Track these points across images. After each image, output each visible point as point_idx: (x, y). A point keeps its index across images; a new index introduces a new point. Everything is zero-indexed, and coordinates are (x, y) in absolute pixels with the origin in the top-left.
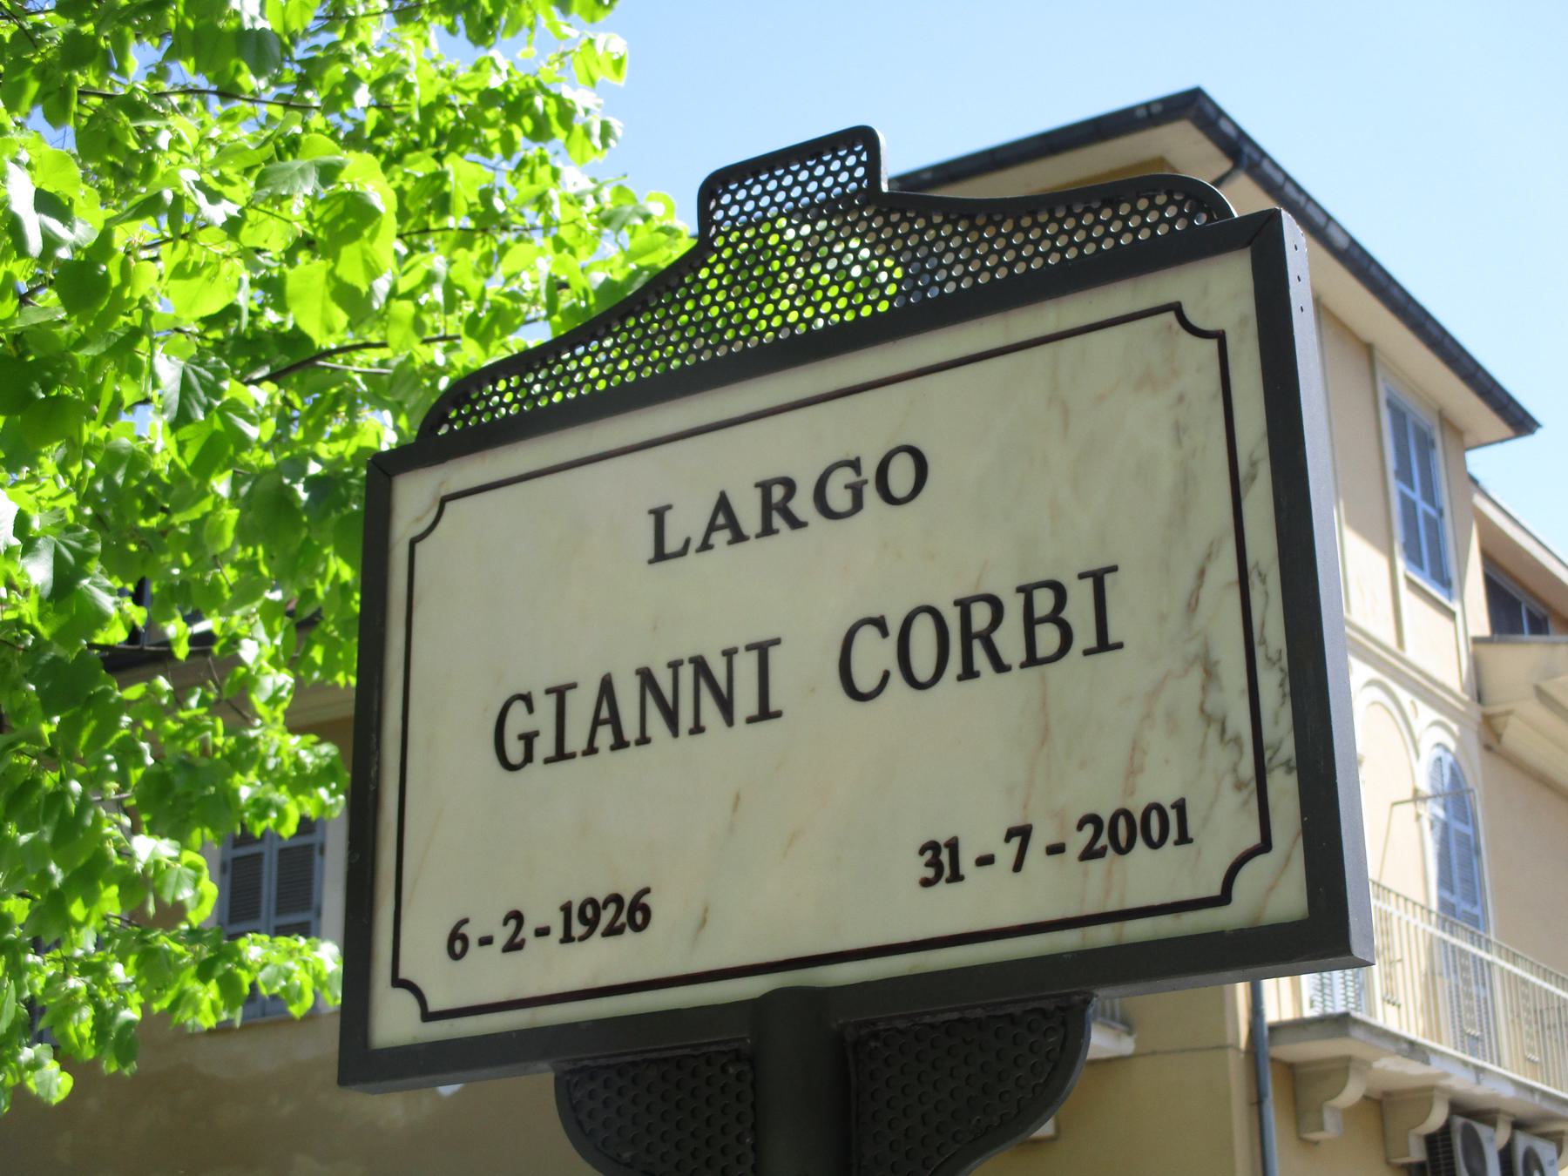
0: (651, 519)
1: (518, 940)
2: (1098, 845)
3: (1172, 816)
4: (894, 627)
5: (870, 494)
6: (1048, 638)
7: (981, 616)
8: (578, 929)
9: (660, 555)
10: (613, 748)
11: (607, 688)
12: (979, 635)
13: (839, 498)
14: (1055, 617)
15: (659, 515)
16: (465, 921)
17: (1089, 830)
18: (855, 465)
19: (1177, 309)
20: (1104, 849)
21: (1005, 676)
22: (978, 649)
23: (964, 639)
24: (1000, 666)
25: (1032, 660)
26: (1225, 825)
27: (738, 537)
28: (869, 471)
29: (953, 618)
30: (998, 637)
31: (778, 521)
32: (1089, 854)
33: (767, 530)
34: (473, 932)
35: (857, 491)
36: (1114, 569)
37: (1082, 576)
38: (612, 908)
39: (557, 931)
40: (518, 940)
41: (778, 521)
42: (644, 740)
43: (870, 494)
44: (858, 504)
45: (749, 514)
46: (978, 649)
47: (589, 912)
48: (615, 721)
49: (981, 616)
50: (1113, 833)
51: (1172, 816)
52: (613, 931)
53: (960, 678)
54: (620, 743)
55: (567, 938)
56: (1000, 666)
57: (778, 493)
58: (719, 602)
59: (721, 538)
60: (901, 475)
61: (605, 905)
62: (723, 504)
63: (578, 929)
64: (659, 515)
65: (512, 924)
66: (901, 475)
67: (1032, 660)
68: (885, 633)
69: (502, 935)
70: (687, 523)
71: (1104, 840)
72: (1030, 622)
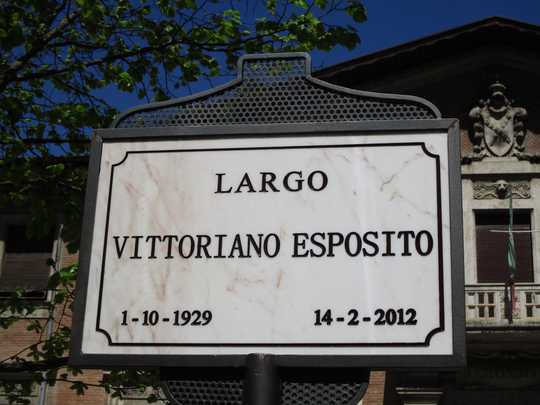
0: (299, 171)
1: (355, 321)
4: (179, 239)
5: (305, 184)
7: (204, 241)
8: (181, 321)
9: (219, 190)
10: (239, 257)
11: (238, 236)
13: (293, 183)
15: (220, 176)
17: (379, 315)
18: (300, 173)
20: (407, 313)
21: (209, 259)
22: (202, 249)
23: (329, 244)
24: (208, 256)
26: (428, 319)
27: (252, 190)
28: (305, 177)
29: (196, 240)
30: (208, 248)
31: (268, 187)
33: (264, 190)
34: (334, 316)
35: (300, 182)
36: (226, 236)
37: (216, 236)
38: (196, 315)
39: (142, 320)
40: (355, 321)
41: (268, 187)
42: (249, 256)
43: (305, 184)
44: (300, 187)
45: (257, 183)
46: (202, 249)
47: (186, 316)
48: (240, 248)
49: (204, 241)
50: (387, 317)
52: (195, 323)
53: (196, 257)
54: (241, 255)
56: (208, 256)
57: (268, 178)
59: (245, 189)
60: (318, 181)
61: (193, 314)
62: (246, 177)
63: (181, 321)
64: (220, 176)
65: (352, 315)
66: (318, 181)
67: (220, 256)
68: (177, 240)
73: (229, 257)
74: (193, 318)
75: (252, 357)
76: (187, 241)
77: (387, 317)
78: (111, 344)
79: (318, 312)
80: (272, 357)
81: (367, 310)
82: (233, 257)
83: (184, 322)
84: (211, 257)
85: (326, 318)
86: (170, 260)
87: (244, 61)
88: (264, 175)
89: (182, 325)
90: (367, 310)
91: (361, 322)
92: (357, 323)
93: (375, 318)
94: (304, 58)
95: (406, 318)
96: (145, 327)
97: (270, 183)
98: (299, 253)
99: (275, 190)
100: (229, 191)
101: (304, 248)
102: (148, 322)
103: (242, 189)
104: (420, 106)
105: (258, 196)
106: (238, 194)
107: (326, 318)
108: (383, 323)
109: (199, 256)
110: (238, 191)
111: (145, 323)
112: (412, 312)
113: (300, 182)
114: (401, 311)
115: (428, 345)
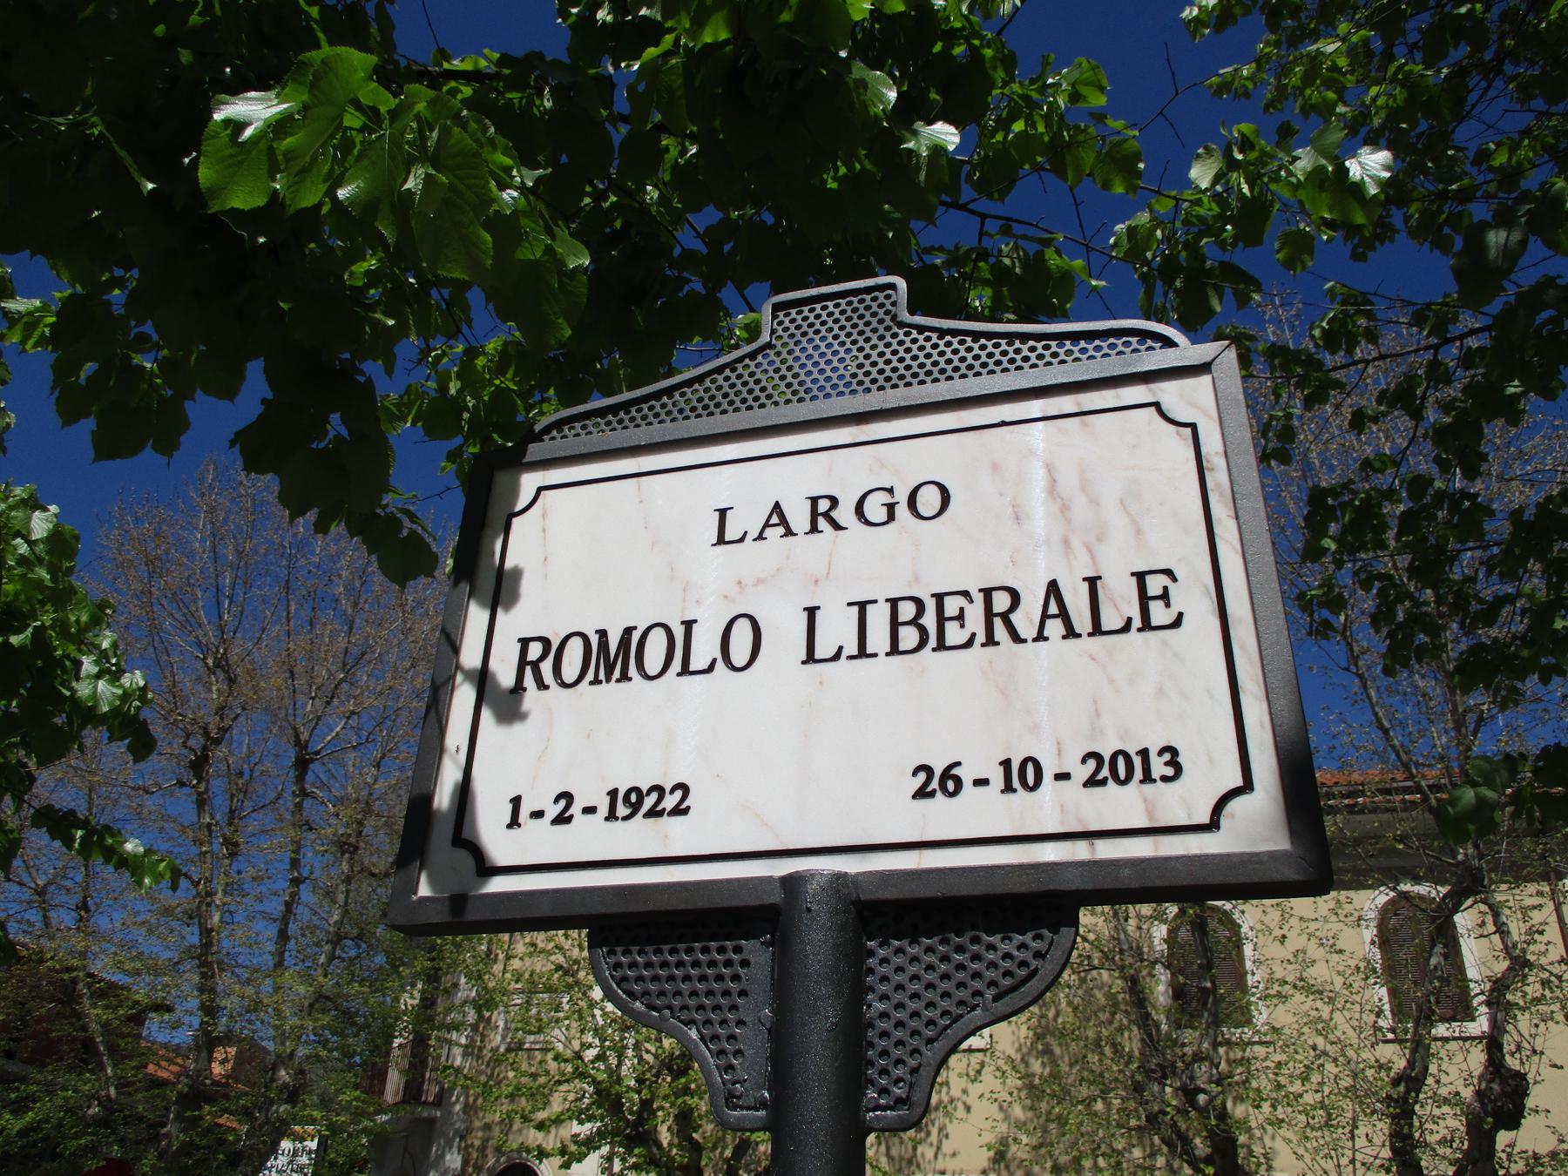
1: (683, 806)
2: (1100, 777)
3: (1137, 761)
5: (902, 511)
6: (909, 637)
8: (622, 810)
9: (721, 540)
11: (1053, 588)
12: (531, 663)
13: (874, 509)
14: (914, 622)
15: (723, 513)
16: (958, 764)
17: (1092, 764)
18: (890, 491)
19: (1157, 405)
20: (1160, 753)
21: (1072, 642)
23: (921, 624)
24: (1016, 638)
25: (894, 650)
27: (789, 533)
28: (902, 496)
31: (822, 523)
32: (1092, 782)
33: (814, 529)
34: (967, 774)
35: (891, 508)
38: (654, 796)
39: (603, 810)
40: (683, 806)
41: (822, 523)
43: (902, 511)
44: (891, 517)
45: (799, 517)
46: (998, 622)
47: (633, 798)
48: (1064, 614)
50: (1111, 768)
51: (1137, 761)
52: (654, 813)
54: (1071, 633)
55: (612, 816)
56: (1016, 638)
58: (707, 589)
59: (774, 533)
60: (929, 500)
62: (777, 506)
63: (622, 810)
64: (723, 513)
66: (929, 500)
67: (894, 650)
69: (553, 811)
70: (744, 521)
71: (1105, 772)
72: (895, 624)
73: (1035, 640)
74: (649, 802)
75: (792, 883)
76: (653, 666)
77: (1111, 768)
78: (1247, 786)
79: (516, 801)
80: (840, 877)
81: (591, 792)
82: (1046, 639)
83: (627, 811)
84: (1025, 641)
85: (938, 782)
86: (1042, 643)
87: (776, 308)
88: (814, 501)
89: (625, 818)
90: (591, 792)
91: (579, 818)
92: (569, 820)
93: (1083, 772)
94: (893, 286)
95: (670, 802)
96: (1010, 796)
97: (827, 515)
98: (1156, 620)
99: (837, 526)
100: (741, 540)
101: (1168, 605)
102: (1016, 783)
103: (769, 532)
104: (1144, 335)
105: (803, 544)
106: (759, 543)
107: (938, 782)
108: (1104, 782)
109: (625, 677)
110: (760, 537)
111: (1008, 788)
112: (684, 788)
113: (891, 508)
114: (1144, 753)
115: (1218, 828)
